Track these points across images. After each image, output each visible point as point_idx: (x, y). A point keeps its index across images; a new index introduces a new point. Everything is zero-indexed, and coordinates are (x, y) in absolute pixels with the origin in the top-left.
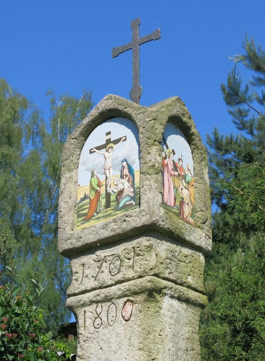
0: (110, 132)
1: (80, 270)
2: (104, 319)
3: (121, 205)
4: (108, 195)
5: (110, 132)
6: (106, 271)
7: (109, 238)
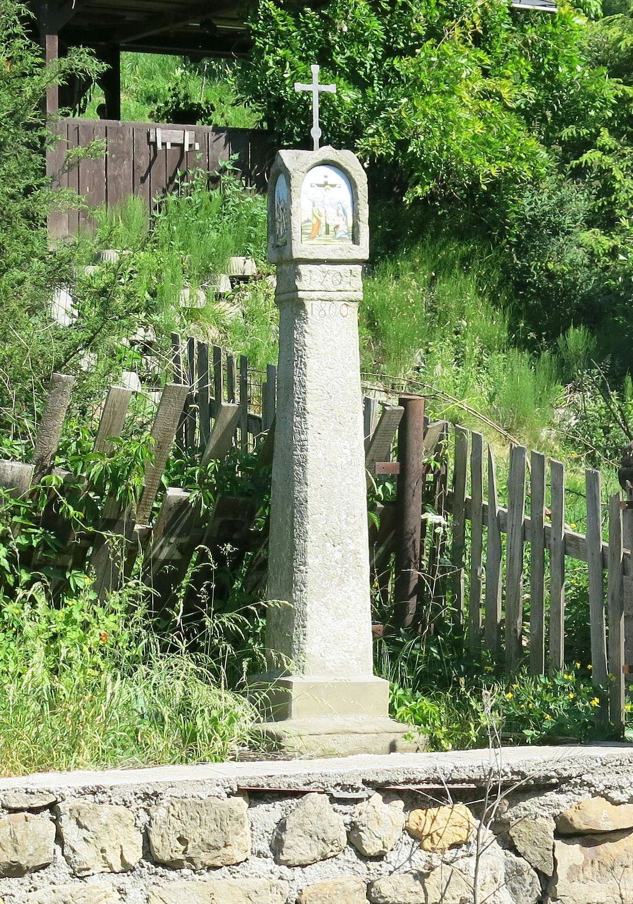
0: (358, 244)
1: (308, 274)
2: (327, 312)
3: (338, 236)
4: (327, 226)
5: (358, 244)
6: (330, 281)
7: (288, 214)
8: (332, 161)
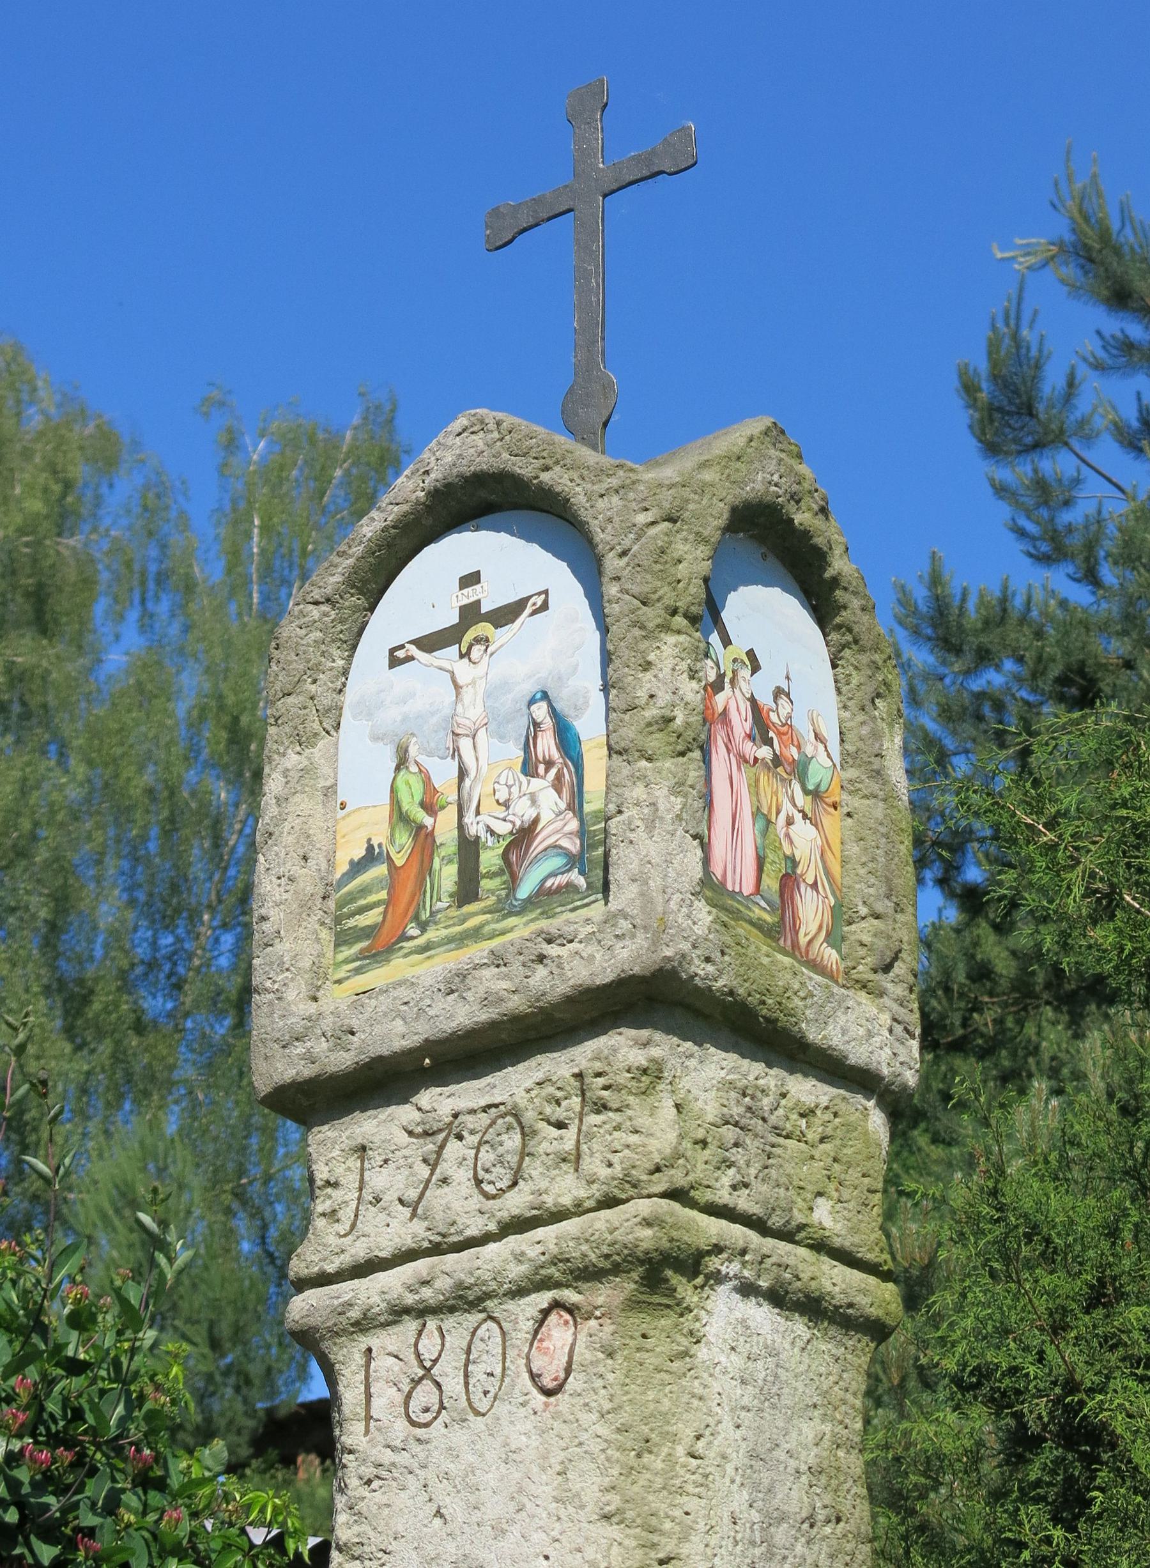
1: (346, 1171)
2: (453, 1385)
3: (525, 891)
6: (462, 1176)
8: (479, 479)
